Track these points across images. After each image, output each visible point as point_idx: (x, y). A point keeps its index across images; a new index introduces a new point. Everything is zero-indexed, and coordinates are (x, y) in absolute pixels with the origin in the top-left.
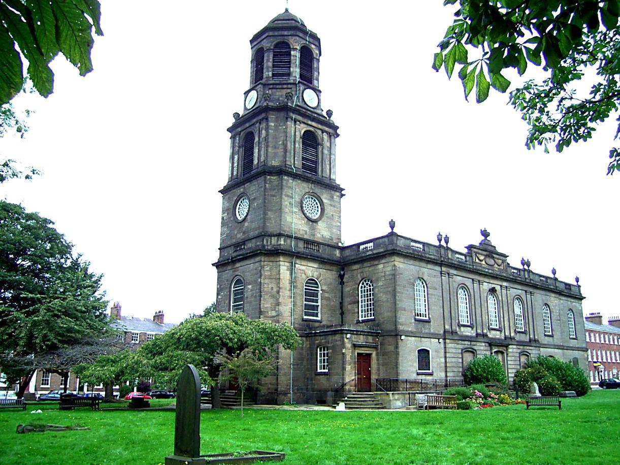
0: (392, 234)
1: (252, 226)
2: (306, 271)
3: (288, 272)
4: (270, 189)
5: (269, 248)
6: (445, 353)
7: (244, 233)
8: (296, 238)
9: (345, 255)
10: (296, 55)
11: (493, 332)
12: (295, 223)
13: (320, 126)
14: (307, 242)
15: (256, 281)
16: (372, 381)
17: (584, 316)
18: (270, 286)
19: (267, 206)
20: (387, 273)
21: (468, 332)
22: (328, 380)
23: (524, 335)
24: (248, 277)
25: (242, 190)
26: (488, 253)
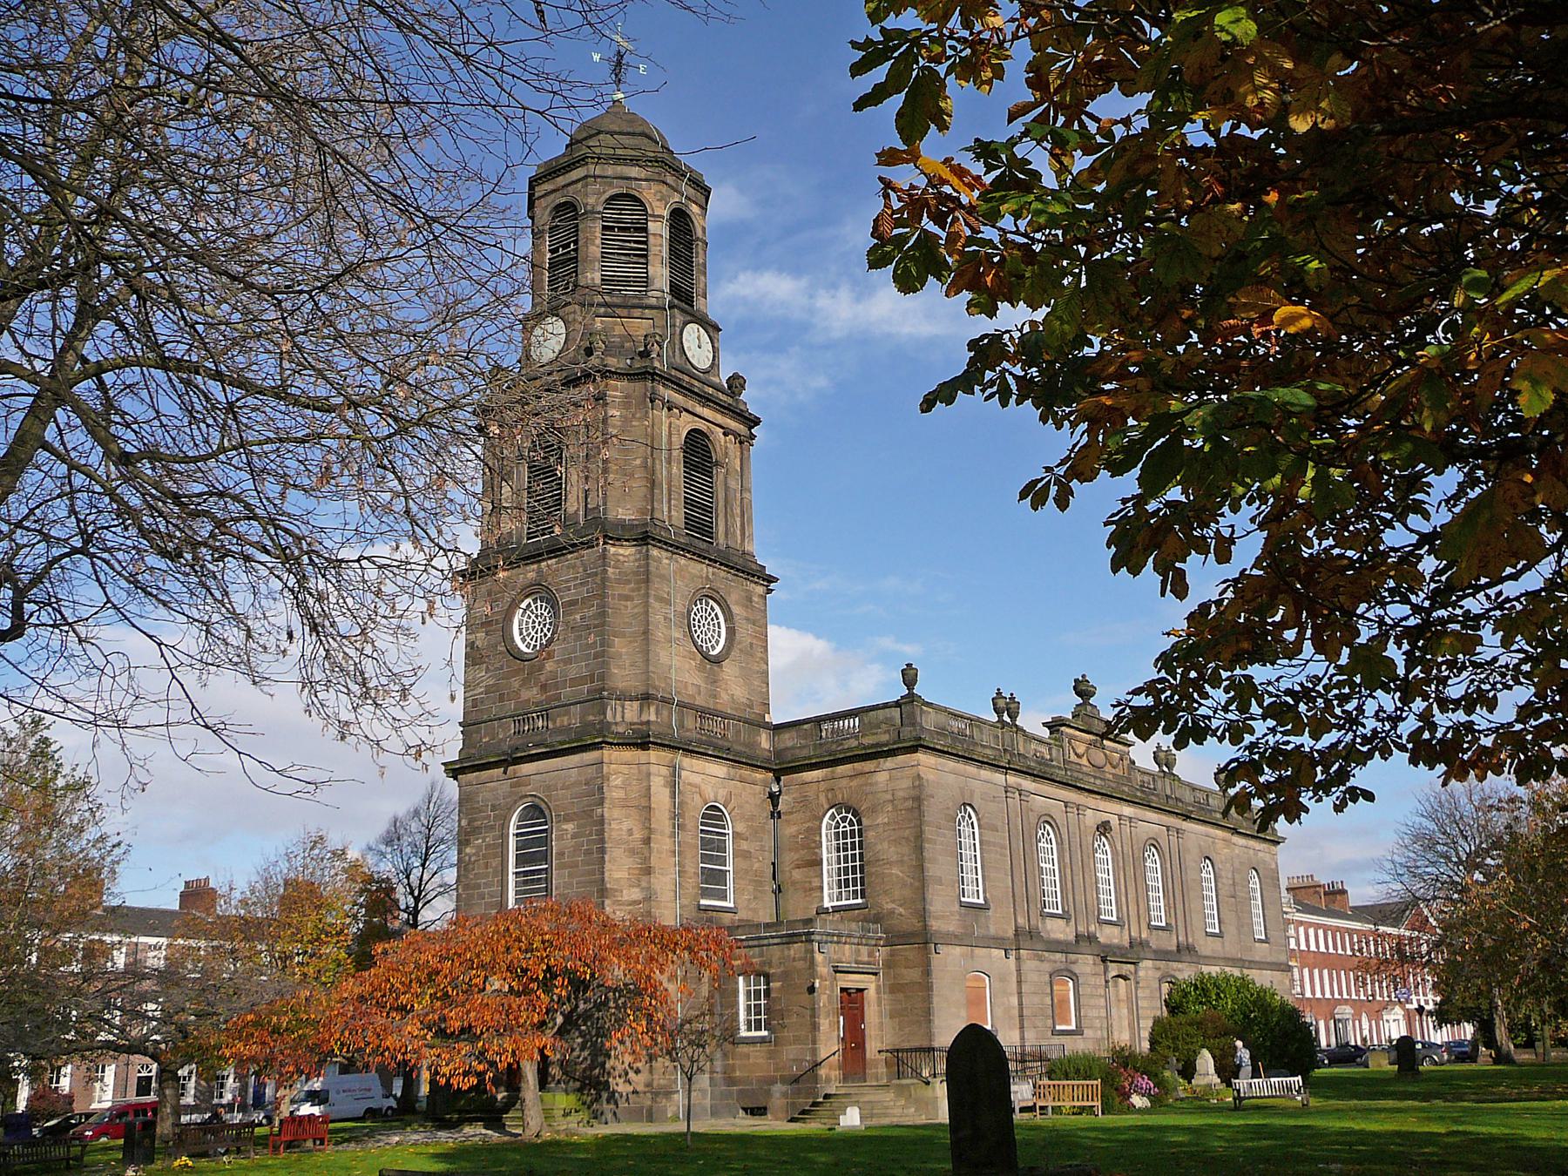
0: (911, 698)
1: (566, 668)
2: (703, 787)
3: (667, 791)
4: (618, 581)
5: (621, 730)
6: (1019, 982)
7: (544, 687)
8: (681, 705)
9: (782, 746)
10: (659, 230)
11: (1108, 929)
12: (678, 670)
13: (719, 418)
14: (704, 713)
15: (588, 814)
16: (868, 1055)
17: (1284, 884)
18: (625, 826)
19: (588, 620)
20: (901, 794)
21: (1059, 931)
22: (771, 1055)
23: (1061, 922)
24: (561, 800)
25: (532, 575)
26: (1092, 737)
